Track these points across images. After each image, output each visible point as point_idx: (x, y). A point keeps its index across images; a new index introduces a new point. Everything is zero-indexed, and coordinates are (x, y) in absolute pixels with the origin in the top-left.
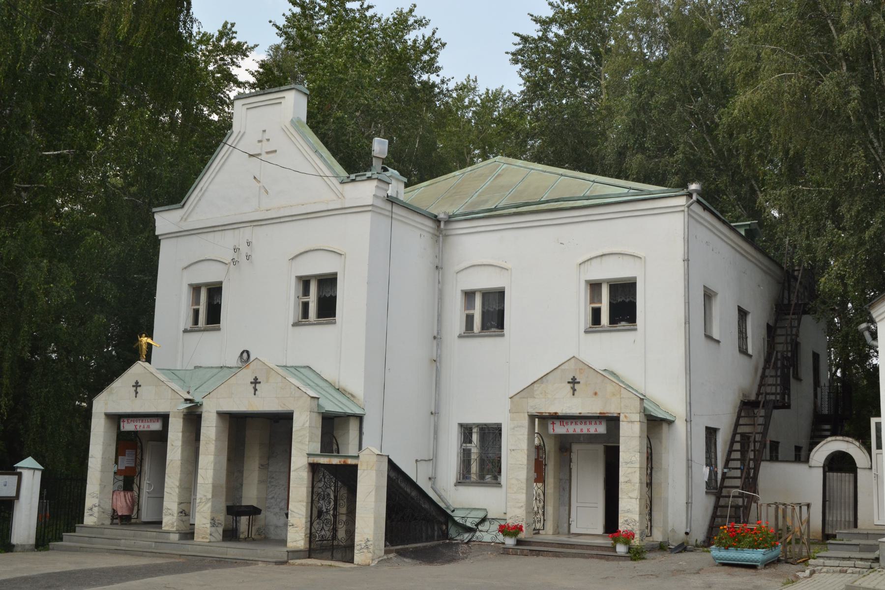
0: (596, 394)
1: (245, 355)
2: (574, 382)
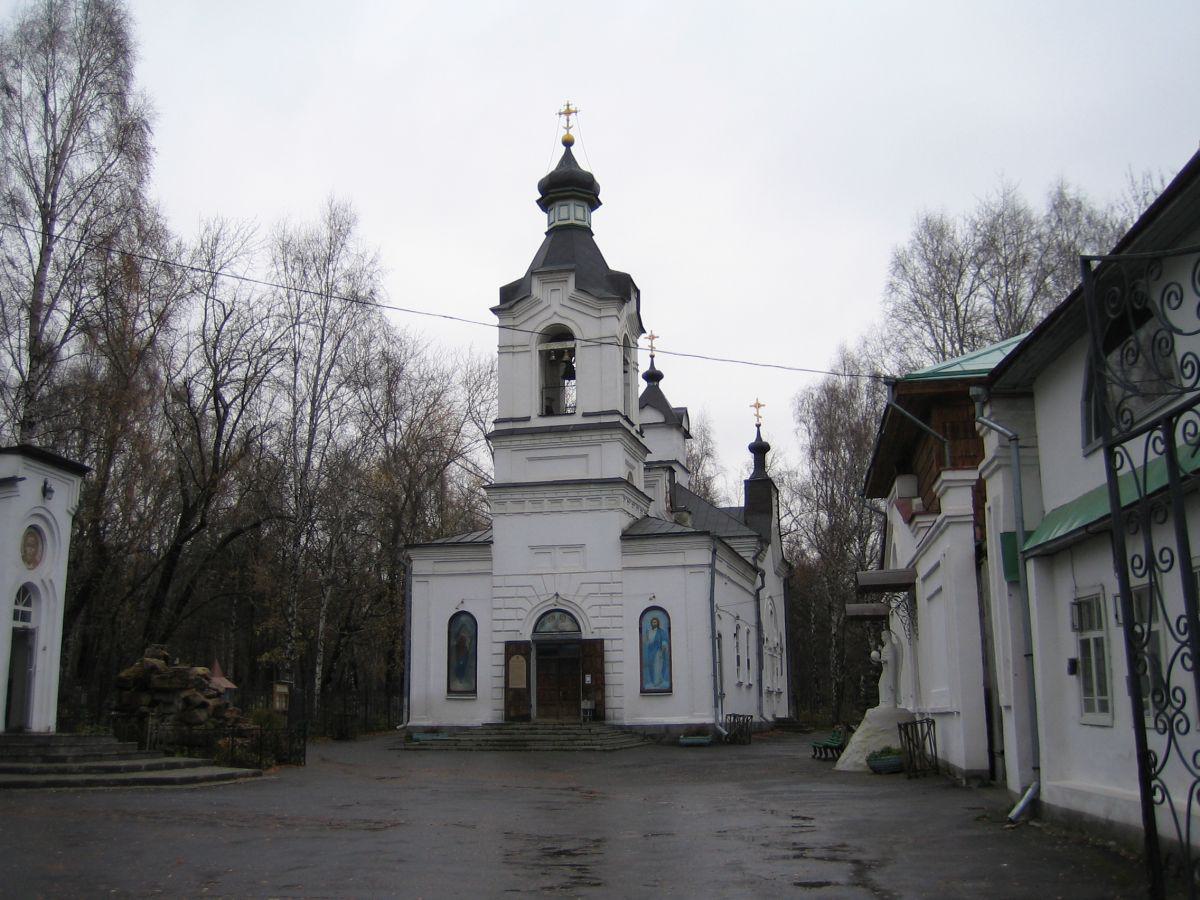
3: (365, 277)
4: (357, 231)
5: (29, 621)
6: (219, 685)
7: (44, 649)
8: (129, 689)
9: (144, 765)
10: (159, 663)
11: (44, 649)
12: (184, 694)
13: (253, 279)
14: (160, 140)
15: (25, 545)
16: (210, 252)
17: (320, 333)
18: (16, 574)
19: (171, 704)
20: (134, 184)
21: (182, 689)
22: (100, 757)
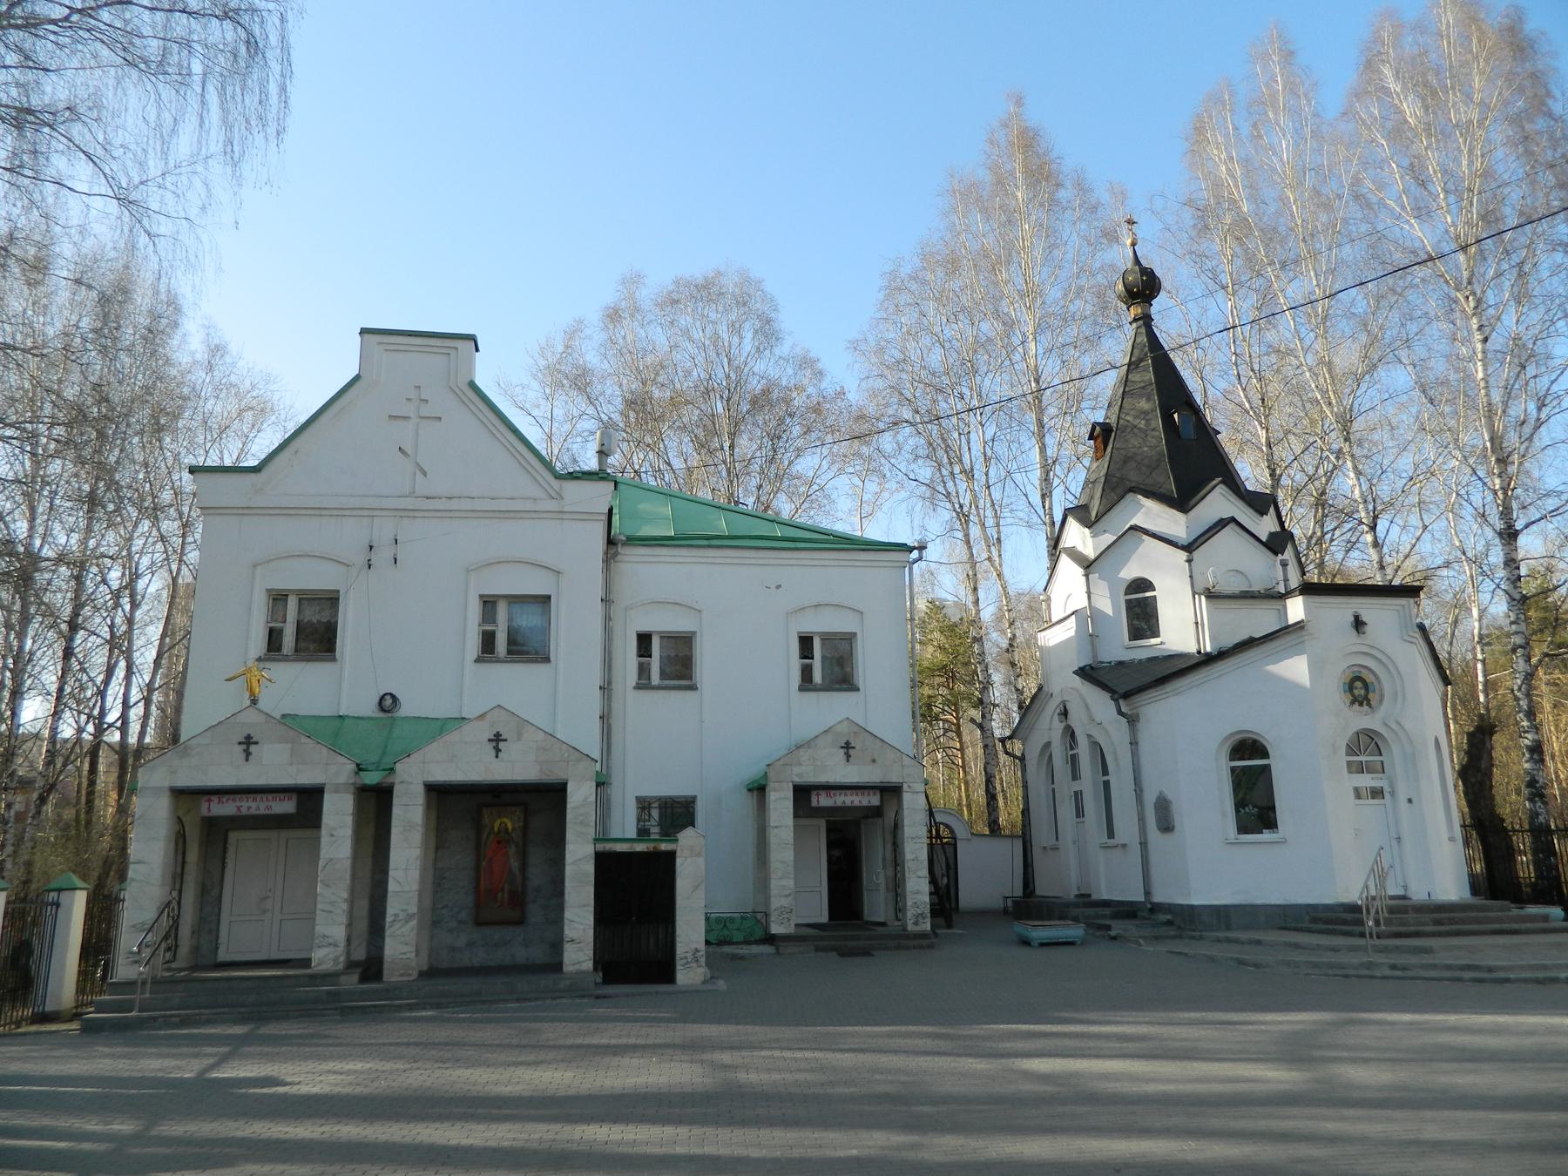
1: (389, 701)
2: (248, 741)
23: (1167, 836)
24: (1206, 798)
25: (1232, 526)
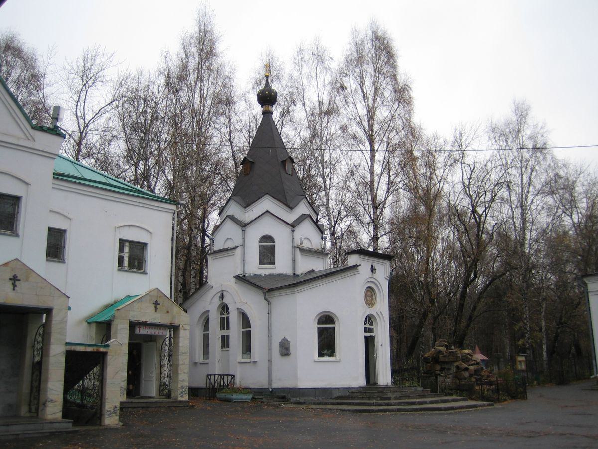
0: (168, 312)
3: (539, 137)
4: (532, 113)
5: (373, 333)
6: (477, 358)
7: (382, 345)
8: (429, 363)
9: (430, 401)
10: (443, 349)
11: (382, 345)
12: (457, 363)
13: (482, 151)
14: (416, 94)
15: (366, 296)
16: (459, 142)
17: (520, 170)
18: (364, 311)
19: (449, 369)
20: (407, 116)
21: (454, 362)
22: (409, 397)
23: (286, 359)
24: (307, 340)
25: (268, 213)
